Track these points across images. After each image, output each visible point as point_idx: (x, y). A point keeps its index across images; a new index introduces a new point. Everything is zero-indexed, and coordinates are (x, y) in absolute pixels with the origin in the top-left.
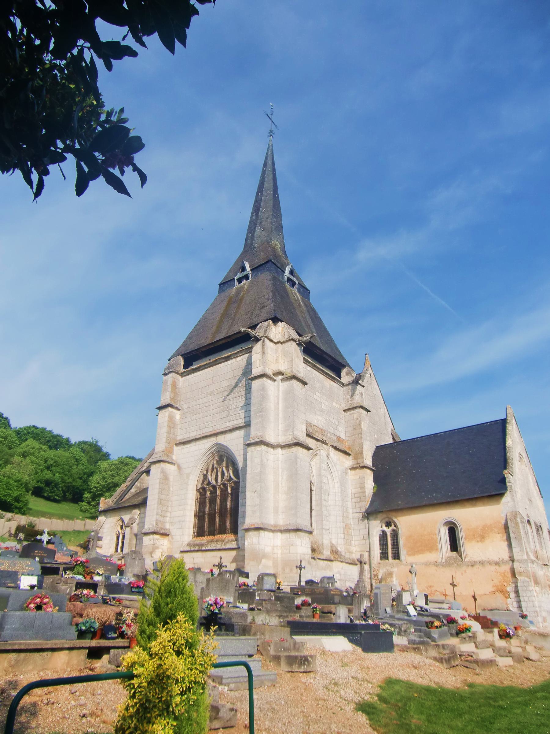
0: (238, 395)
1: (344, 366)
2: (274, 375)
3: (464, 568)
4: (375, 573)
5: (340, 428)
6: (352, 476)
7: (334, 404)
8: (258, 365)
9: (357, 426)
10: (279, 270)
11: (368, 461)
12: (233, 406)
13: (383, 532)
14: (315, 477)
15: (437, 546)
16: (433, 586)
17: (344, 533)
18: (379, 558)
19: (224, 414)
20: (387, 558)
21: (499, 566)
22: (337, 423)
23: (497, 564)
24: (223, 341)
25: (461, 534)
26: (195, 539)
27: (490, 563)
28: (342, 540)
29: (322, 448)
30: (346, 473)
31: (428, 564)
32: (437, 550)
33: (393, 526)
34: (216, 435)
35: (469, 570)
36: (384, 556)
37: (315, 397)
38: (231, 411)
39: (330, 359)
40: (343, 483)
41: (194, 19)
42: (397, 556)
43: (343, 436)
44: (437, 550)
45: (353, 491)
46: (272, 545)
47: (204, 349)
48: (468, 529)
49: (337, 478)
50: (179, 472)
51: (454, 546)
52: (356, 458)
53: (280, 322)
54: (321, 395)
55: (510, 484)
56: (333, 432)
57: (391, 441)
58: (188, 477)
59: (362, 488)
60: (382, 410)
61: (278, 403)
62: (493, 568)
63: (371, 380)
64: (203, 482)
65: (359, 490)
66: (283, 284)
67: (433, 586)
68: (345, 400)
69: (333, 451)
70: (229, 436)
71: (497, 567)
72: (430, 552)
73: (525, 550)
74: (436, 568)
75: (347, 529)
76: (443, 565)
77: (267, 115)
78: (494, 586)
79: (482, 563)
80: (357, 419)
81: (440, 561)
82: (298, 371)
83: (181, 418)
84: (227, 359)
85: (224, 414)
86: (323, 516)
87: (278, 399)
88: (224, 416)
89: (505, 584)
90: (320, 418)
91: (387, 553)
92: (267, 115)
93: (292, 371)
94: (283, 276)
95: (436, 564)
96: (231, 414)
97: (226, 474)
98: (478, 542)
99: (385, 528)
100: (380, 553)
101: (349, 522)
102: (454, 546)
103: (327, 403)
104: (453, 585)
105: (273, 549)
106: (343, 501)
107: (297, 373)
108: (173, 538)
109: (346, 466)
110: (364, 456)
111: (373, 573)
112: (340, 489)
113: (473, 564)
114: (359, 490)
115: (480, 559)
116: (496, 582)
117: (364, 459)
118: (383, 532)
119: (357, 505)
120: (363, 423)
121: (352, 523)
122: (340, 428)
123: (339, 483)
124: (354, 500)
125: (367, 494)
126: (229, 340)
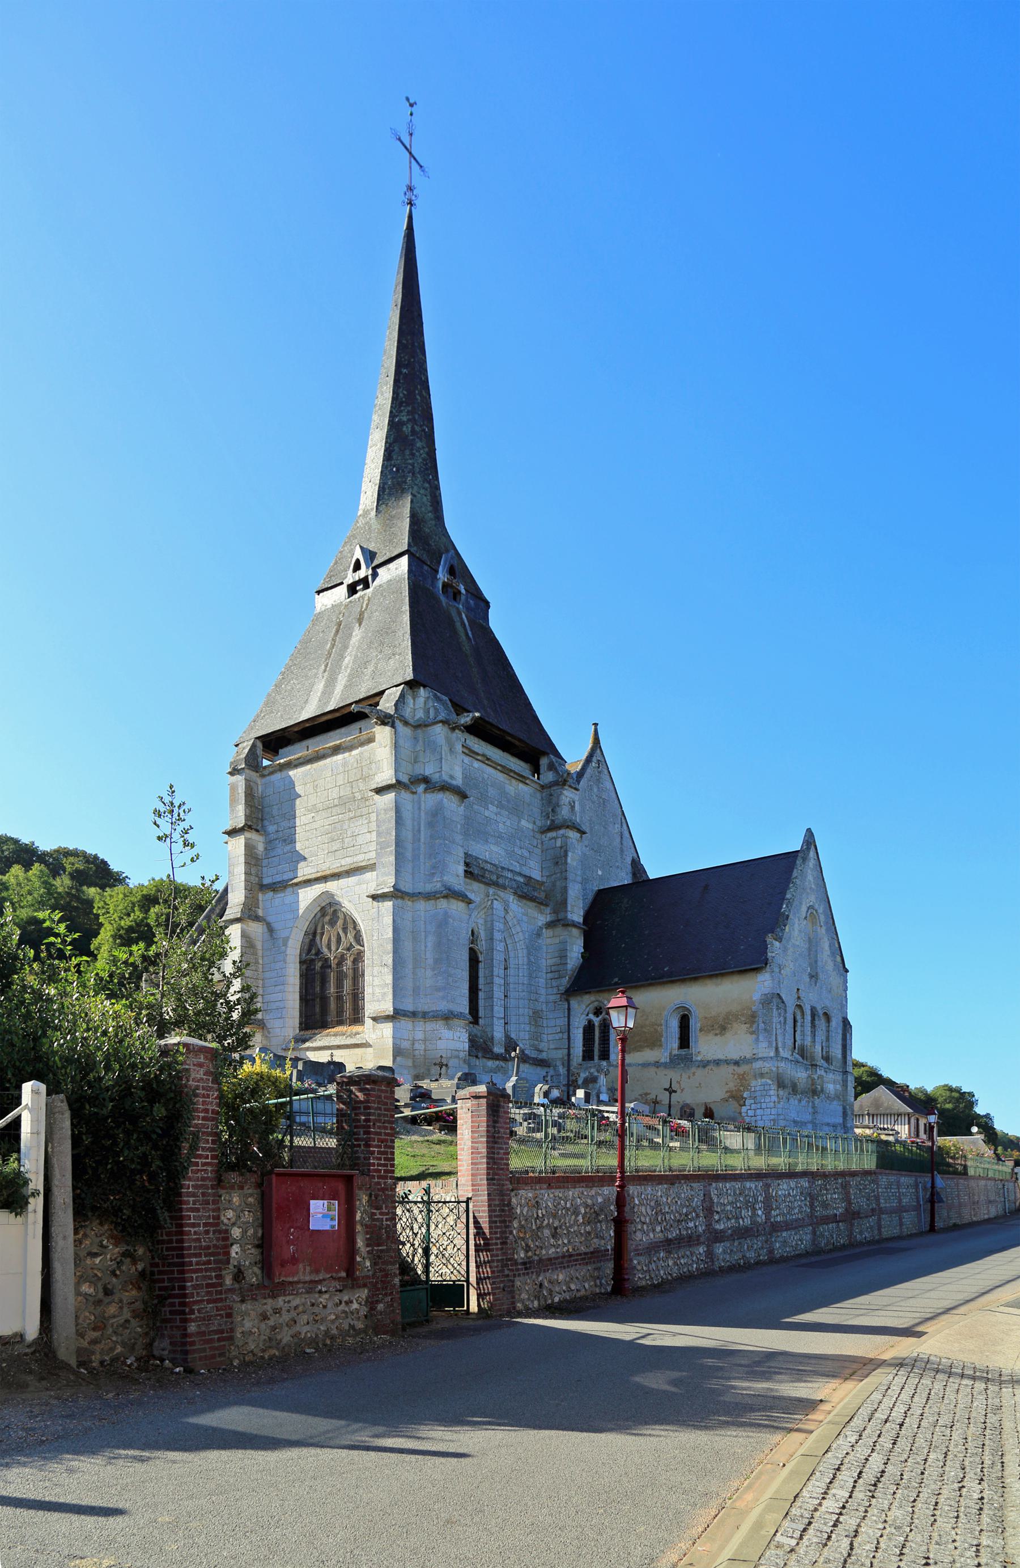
0: (357, 815)
1: (544, 754)
2: (412, 783)
3: (693, 1069)
4: (574, 1078)
5: (531, 862)
6: (549, 939)
7: (523, 823)
8: (385, 769)
9: (558, 860)
10: (426, 568)
11: (576, 914)
12: (349, 833)
13: (590, 1021)
14: (484, 942)
15: (661, 1041)
16: (649, 1094)
17: (530, 1024)
18: (581, 1058)
19: (336, 845)
20: (591, 1058)
21: (739, 1066)
22: (526, 854)
23: (737, 1063)
24: (329, 717)
25: (694, 1025)
26: (302, 1033)
27: (727, 1062)
28: (527, 1033)
29: (496, 897)
30: (539, 935)
31: (645, 1065)
32: (661, 1046)
33: (604, 1013)
34: (324, 879)
35: (700, 1072)
36: (588, 1055)
37: (487, 813)
38: (346, 840)
39: (517, 743)
40: (532, 949)
41: (298, 802)
42: (605, 1055)
43: (536, 875)
44: (661, 1046)
45: (550, 962)
46: (411, 1039)
47: (296, 729)
48: (706, 1018)
49: (522, 942)
50: (271, 936)
51: (684, 1041)
52: (555, 912)
53: (422, 688)
54: (499, 810)
55: (773, 955)
56: (518, 870)
57: (627, 880)
58: (285, 944)
59: (563, 955)
60: (616, 826)
61: (419, 831)
62: (731, 1068)
63: (600, 772)
64: (309, 950)
65: (557, 960)
66: (434, 597)
67: (649, 1094)
68: (544, 814)
69: (515, 902)
70: (343, 882)
71: (736, 1068)
72: (652, 1049)
73: (774, 1043)
74: (656, 1069)
75: (536, 1017)
76: (665, 1065)
77: (400, 139)
78: (727, 1092)
79: (717, 1063)
80: (561, 847)
81: (663, 1060)
82: (452, 777)
83: (266, 849)
84: (336, 750)
85: (336, 845)
86: (495, 1000)
87: (419, 824)
88: (335, 848)
89: (742, 1088)
90: (494, 848)
91: (593, 1051)
92: (400, 139)
93: (440, 776)
94: (435, 578)
95: (657, 1064)
96: (346, 845)
97: (343, 939)
98: (716, 1035)
99: (591, 1016)
100: (583, 1051)
101: (539, 1008)
102: (684, 1041)
103: (508, 823)
104: (671, 1091)
105: (413, 1044)
106: (530, 976)
107: (449, 781)
108: (269, 1033)
109: (540, 924)
110: (569, 908)
111: (571, 1078)
112: (525, 959)
113: (705, 1064)
114: (557, 960)
115: (716, 1057)
116: (732, 1086)
117: (569, 913)
118: (590, 1021)
119: (554, 984)
120: (570, 854)
121: (544, 1009)
122: (531, 862)
123: (525, 951)
124: (550, 975)
125: (569, 967)
126: (337, 715)
